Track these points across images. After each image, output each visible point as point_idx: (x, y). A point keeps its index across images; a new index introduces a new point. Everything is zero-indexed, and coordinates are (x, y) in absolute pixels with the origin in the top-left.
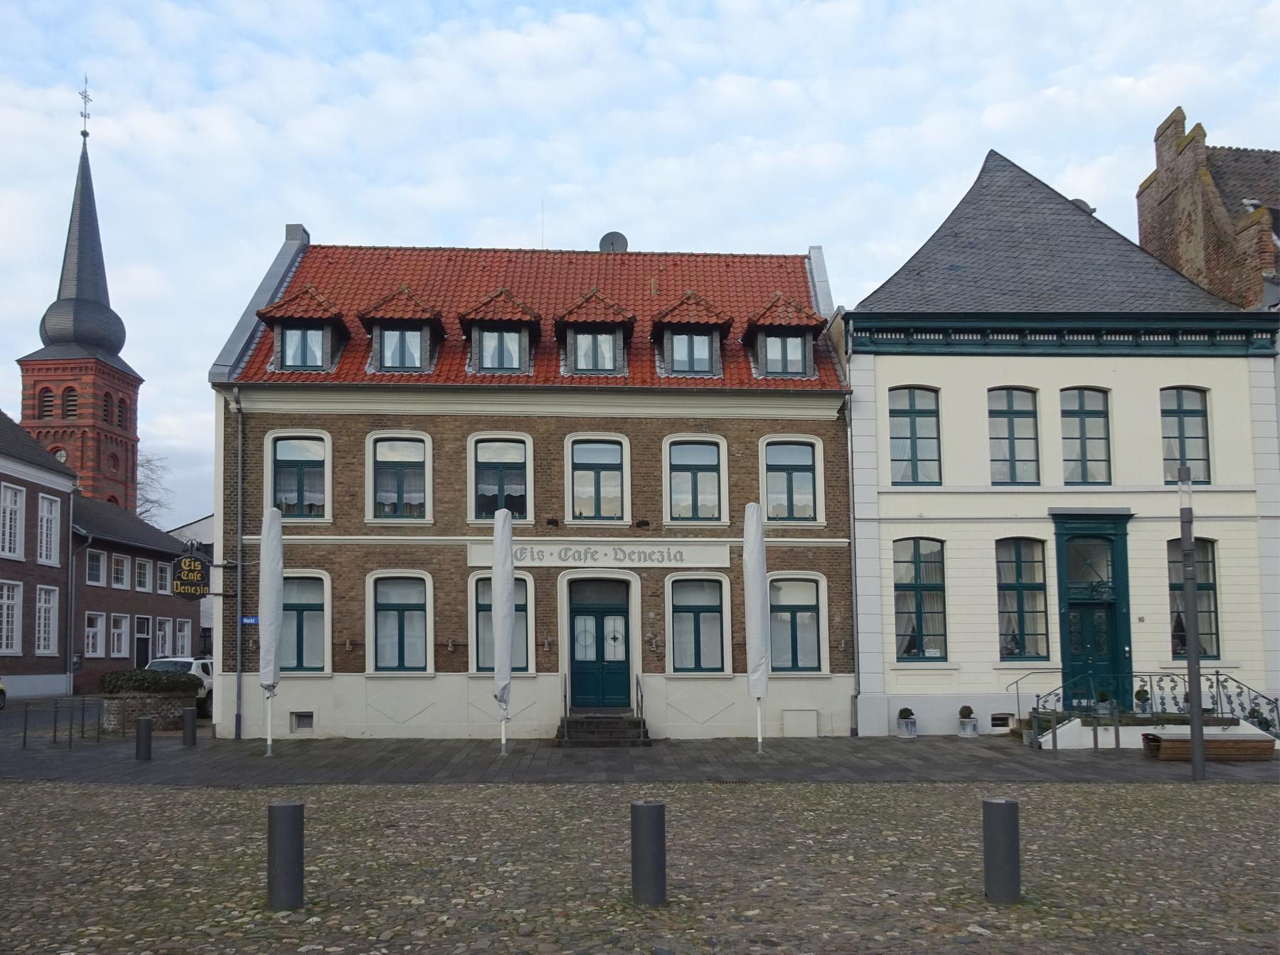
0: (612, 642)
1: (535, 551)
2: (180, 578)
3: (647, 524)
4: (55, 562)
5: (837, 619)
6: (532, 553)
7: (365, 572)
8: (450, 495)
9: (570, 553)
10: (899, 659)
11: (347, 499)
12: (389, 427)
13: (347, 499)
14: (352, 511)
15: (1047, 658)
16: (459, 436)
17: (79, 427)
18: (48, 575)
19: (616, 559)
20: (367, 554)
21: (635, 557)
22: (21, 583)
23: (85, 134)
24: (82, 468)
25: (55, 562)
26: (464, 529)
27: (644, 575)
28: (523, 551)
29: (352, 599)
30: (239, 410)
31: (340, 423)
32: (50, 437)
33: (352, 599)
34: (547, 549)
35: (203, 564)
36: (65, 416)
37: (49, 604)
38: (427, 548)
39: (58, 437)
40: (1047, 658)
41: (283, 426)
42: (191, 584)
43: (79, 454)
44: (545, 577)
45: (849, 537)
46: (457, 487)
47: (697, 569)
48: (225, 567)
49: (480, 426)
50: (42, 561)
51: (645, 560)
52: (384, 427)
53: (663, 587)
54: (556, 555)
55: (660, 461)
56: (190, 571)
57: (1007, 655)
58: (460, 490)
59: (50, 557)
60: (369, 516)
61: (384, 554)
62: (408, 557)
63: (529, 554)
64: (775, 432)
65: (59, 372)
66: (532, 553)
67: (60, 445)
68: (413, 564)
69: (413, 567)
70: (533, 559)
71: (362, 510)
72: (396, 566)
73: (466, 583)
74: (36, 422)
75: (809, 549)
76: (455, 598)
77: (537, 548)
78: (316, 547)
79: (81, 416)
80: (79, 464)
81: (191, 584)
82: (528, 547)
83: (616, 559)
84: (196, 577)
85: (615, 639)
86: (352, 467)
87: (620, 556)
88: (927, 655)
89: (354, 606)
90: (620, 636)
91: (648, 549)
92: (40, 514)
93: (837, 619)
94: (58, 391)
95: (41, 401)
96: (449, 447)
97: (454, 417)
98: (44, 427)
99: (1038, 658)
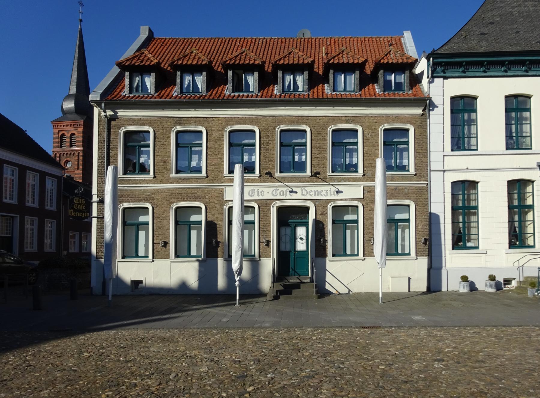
0: (299, 240)
1: (260, 191)
2: (73, 208)
3: (319, 173)
4: (54, 208)
5: (420, 226)
6: (258, 192)
7: (171, 203)
8: (215, 161)
9: (278, 192)
10: (453, 249)
11: (162, 164)
12: (184, 124)
13: (162, 164)
14: (164, 171)
15: (357, 255)
16: (220, 129)
17: (77, 151)
18: (50, 215)
19: (302, 195)
20: (172, 194)
21: (313, 193)
22: (37, 218)
23: (81, 21)
24: (78, 169)
25: (54, 208)
26: (221, 180)
27: (317, 203)
28: (253, 191)
29: (164, 218)
30: (106, 116)
31: (159, 122)
32: (65, 155)
33: (164, 218)
34: (266, 189)
35: (86, 200)
36: (71, 146)
37: (50, 226)
38: (203, 190)
39: (68, 155)
40: (357, 255)
41: (130, 125)
42: (80, 211)
43: (77, 163)
44: (264, 205)
45: (427, 181)
46: (219, 156)
47: (345, 199)
48: (98, 202)
49: (231, 123)
50: (48, 208)
51: (318, 195)
52: (181, 124)
53: (327, 210)
54: (270, 193)
55: (326, 140)
56: (79, 204)
57: (512, 245)
58: (221, 158)
59: (51, 206)
60: (173, 174)
61: (181, 194)
62: (193, 195)
63: (256, 193)
64: (388, 122)
65: (65, 127)
66: (258, 192)
67: (69, 159)
68: (196, 199)
69: (195, 201)
70: (258, 196)
71: (169, 170)
72: (187, 200)
73: (223, 209)
74: (59, 149)
75: (406, 188)
76: (217, 218)
77: (261, 189)
78: (145, 190)
79: (78, 146)
80: (77, 167)
81: (80, 211)
82: (256, 189)
83: (302, 195)
84: (82, 207)
85: (301, 239)
86: (165, 147)
87: (305, 193)
88: (468, 246)
89: (164, 222)
90: (304, 237)
91: (319, 189)
92: (27, 181)
93: (420, 226)
94: (68, 135)
95: (61, 140)
96: (215, 135)
97: (218, 118)
98: (66, 151)
99: (530, 247)
